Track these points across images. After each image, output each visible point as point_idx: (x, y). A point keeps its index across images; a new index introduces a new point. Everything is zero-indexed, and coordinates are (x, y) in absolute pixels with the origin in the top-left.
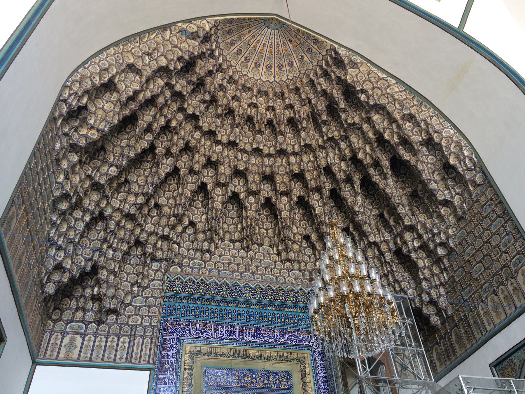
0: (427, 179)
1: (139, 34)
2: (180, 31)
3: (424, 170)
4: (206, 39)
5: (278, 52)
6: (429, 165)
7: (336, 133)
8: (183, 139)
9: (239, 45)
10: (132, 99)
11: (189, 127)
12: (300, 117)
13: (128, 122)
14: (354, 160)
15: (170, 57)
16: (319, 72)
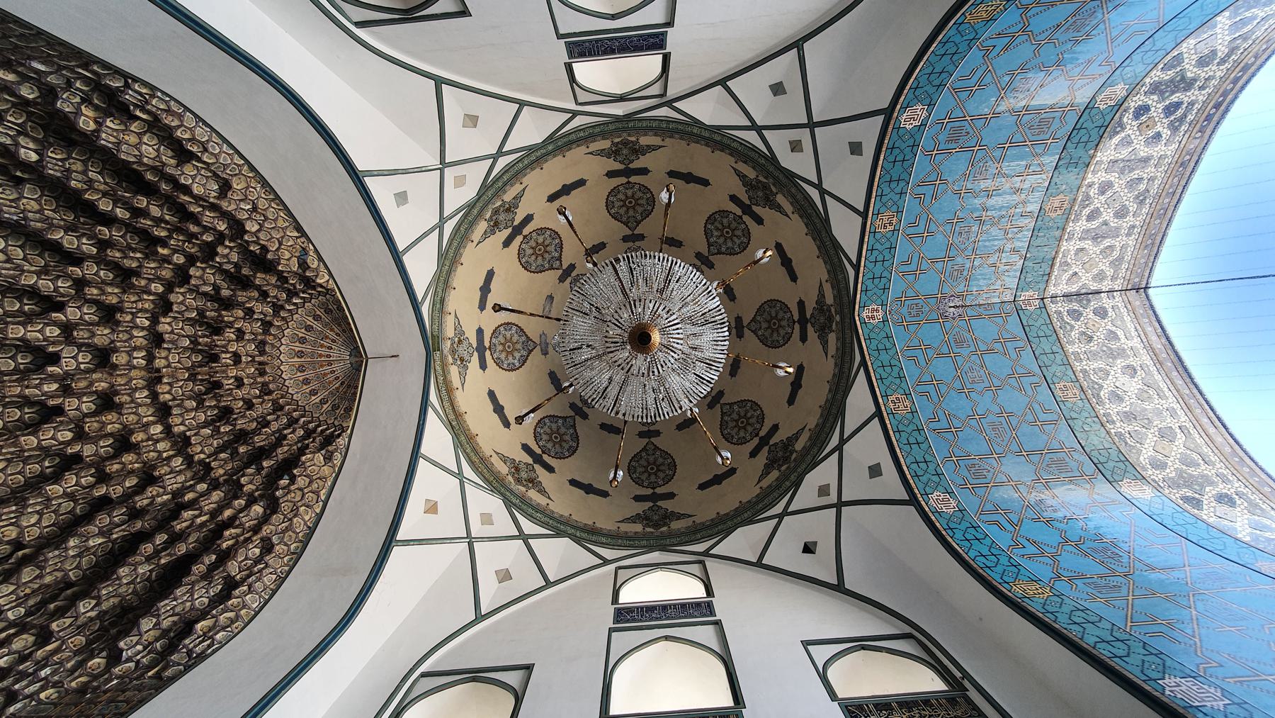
0: (158, 610)
1: (277, 197)
3: (175, 599)
4: (309, 283)
6: (188, 604)
7: (221, 471)
8: (140, 266)
9: (317, 326)
10: (173, 181)
11: (166, 273)
12: (235, 419)
13: (128, 176)
14: (177, 507)
15: (262, 235)
16: (311, 426)
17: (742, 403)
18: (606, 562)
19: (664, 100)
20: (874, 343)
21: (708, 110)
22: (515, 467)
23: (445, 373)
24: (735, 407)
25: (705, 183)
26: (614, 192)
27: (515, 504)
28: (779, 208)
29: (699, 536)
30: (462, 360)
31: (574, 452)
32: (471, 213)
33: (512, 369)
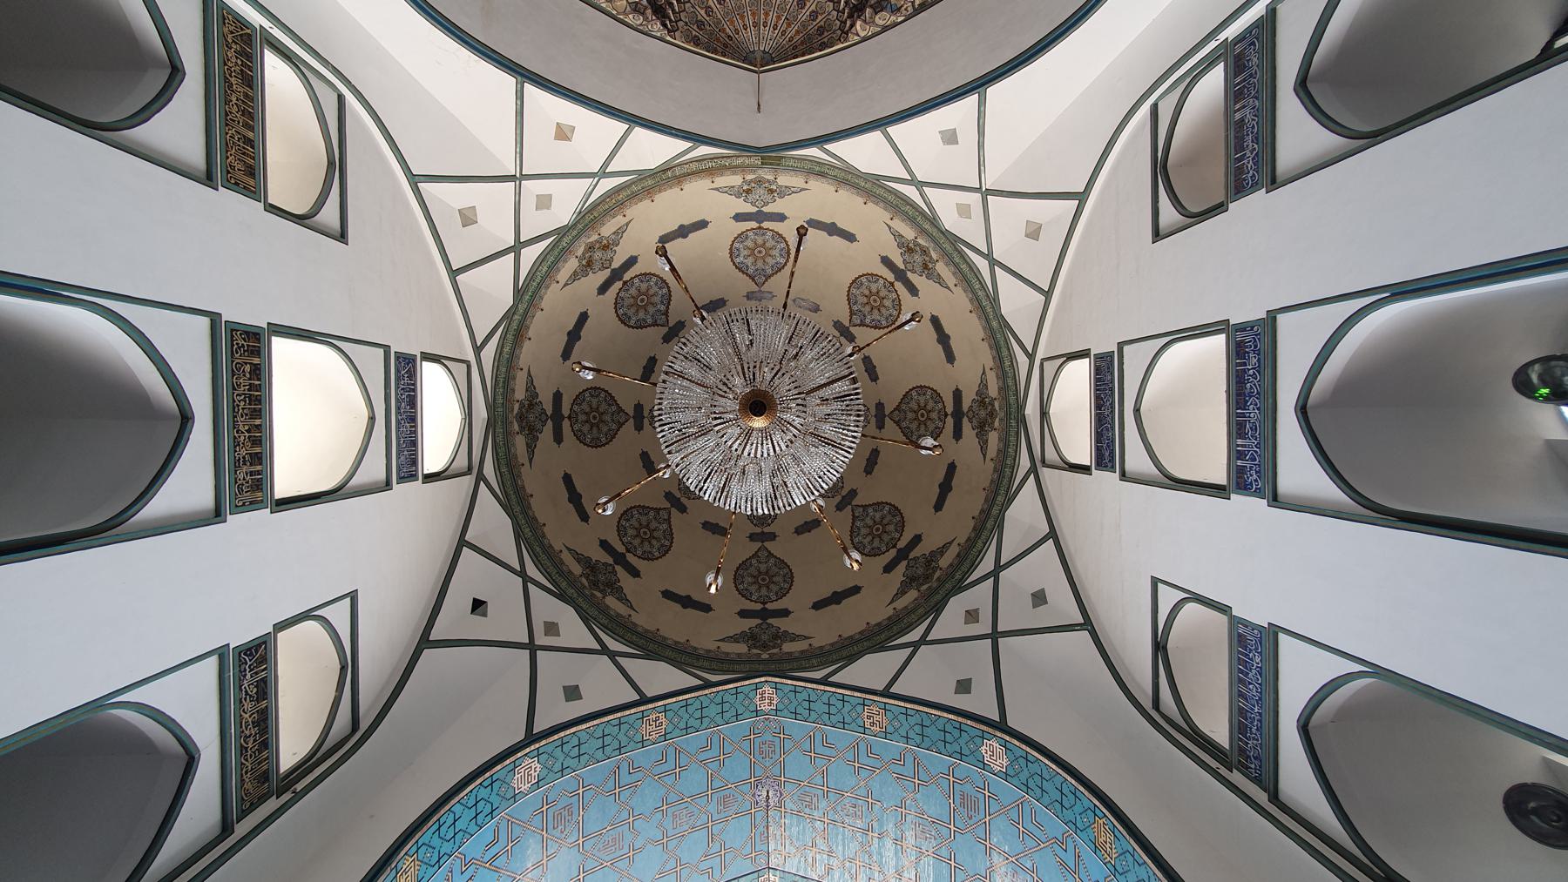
2: (899, 9)
5: (742, 17)
18: (478, 349)
19: (1038, 464)
20: (731, 699)
21: (1023, 513)
23: (733, 169)
25: (938, 507)
26: (937, 395)
27: (562, 240)
28: (901, 592)
29: (504, 470)
30: (748, 192)
32: (926, 221)
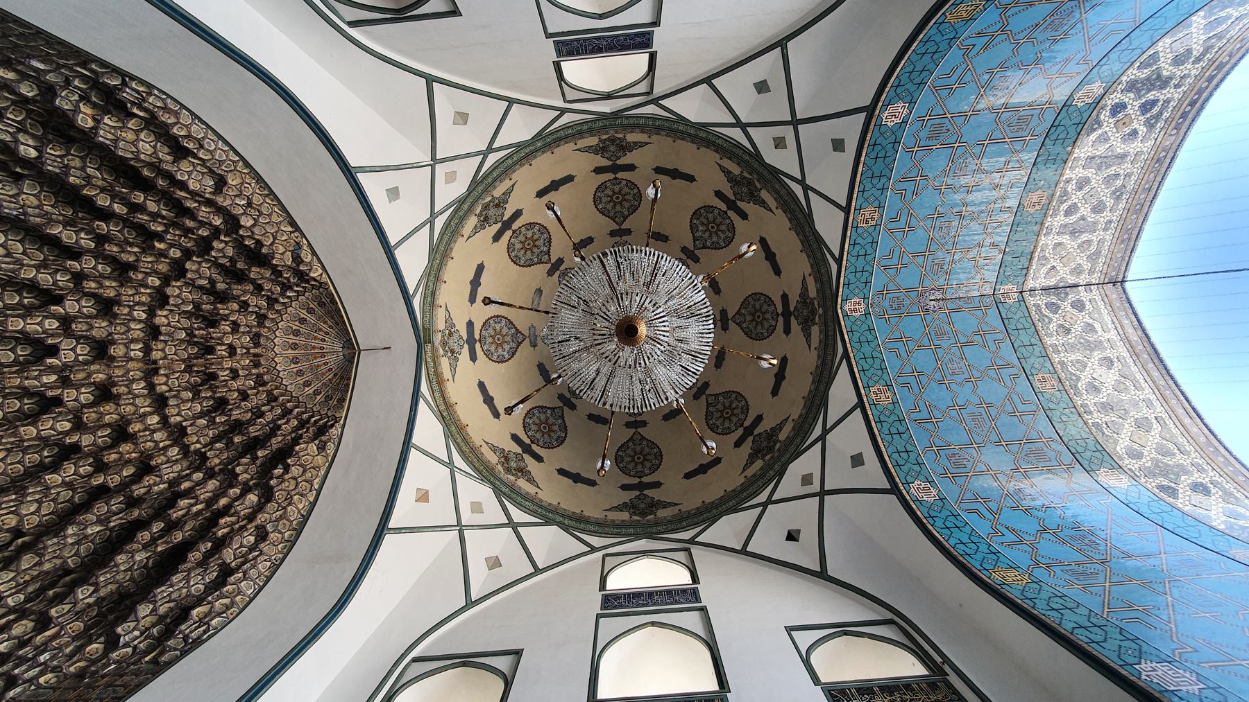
0: (155, 596)
1: (272, 192)
3: (172, 586)
4: (302, 277)
6: (185, 591)
7: (217, 461)
8: (137, 260)
9: (311, 318)
10: (169, 177)
11: (163, 267)
12: (231, 410)
13: (126, 172)
14: (174, 496)
15: (256, 230)
16: (305, 416)
17: (727, 394)
18: (593, 549)
19: (651, 97)
20: (856, 335)
21: (694, 107)
22: (505, 457)
23: (436, 365)
24: (720, 398)
25: (691, 179)
26: (601, 187)
27: (505, 492)
28: (763, 204)
29: (684, 524)
30: (452, 352)
31: (563, 442)
32: (461, 208)
33: (502, 361)
